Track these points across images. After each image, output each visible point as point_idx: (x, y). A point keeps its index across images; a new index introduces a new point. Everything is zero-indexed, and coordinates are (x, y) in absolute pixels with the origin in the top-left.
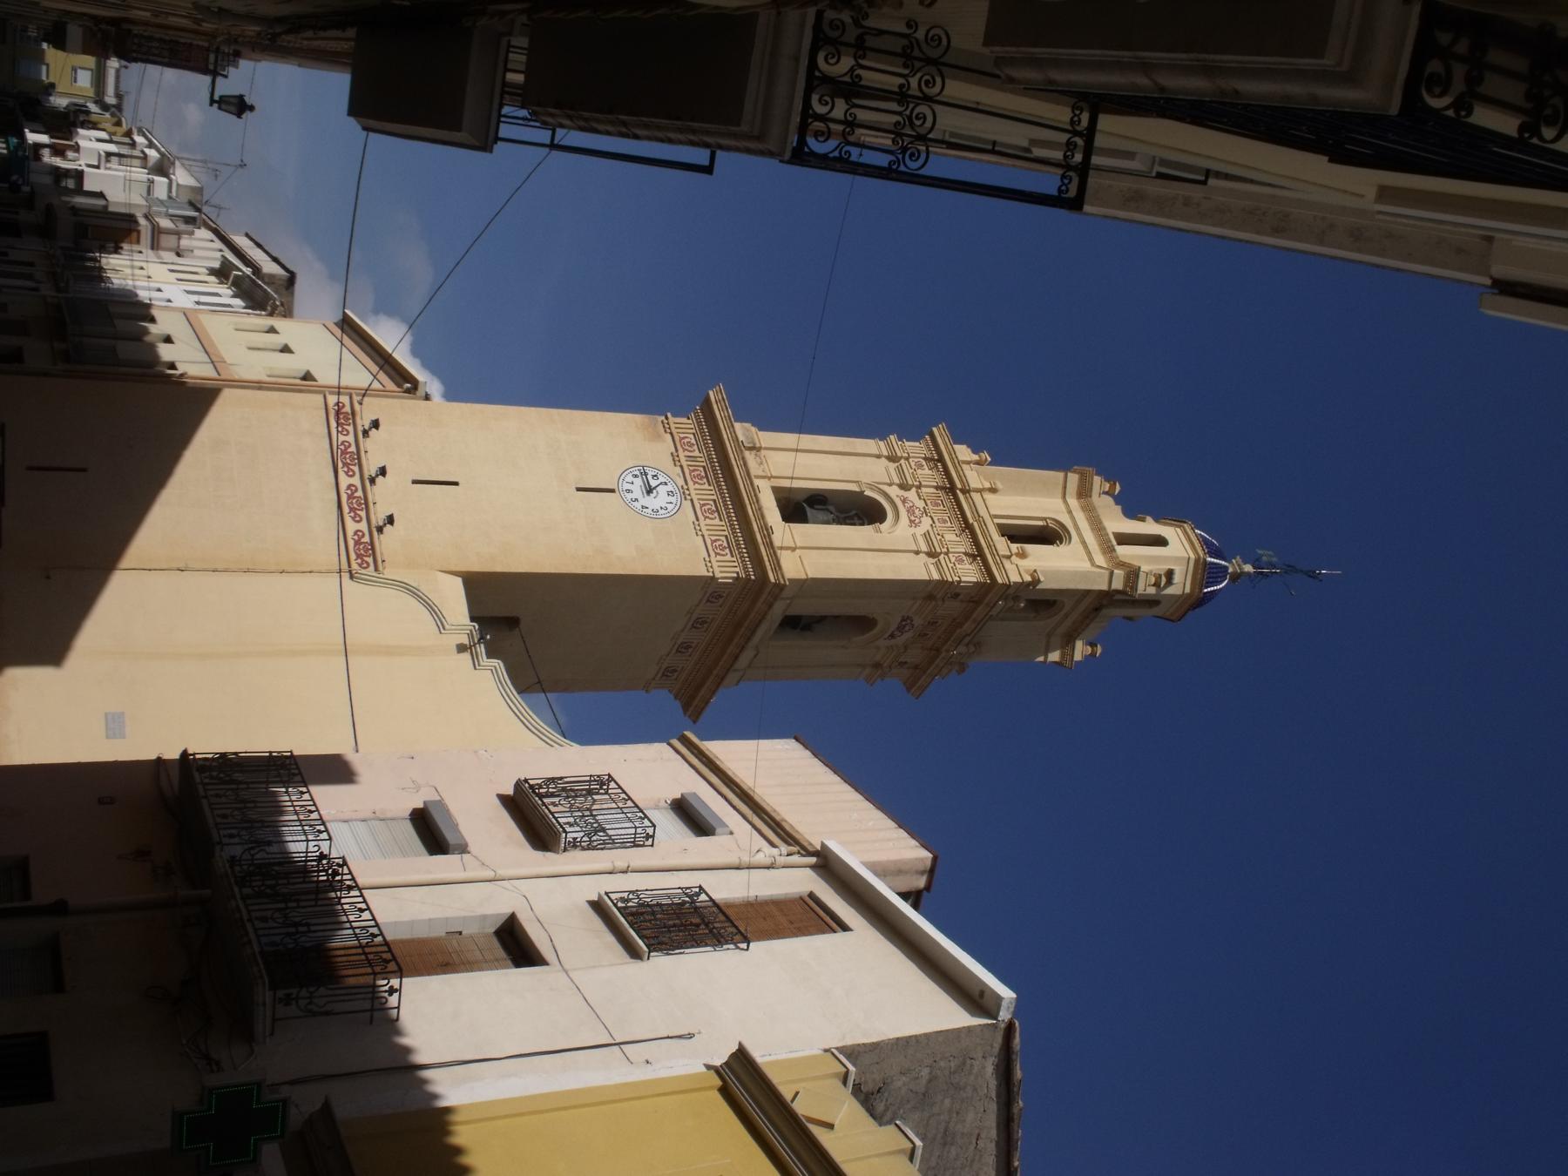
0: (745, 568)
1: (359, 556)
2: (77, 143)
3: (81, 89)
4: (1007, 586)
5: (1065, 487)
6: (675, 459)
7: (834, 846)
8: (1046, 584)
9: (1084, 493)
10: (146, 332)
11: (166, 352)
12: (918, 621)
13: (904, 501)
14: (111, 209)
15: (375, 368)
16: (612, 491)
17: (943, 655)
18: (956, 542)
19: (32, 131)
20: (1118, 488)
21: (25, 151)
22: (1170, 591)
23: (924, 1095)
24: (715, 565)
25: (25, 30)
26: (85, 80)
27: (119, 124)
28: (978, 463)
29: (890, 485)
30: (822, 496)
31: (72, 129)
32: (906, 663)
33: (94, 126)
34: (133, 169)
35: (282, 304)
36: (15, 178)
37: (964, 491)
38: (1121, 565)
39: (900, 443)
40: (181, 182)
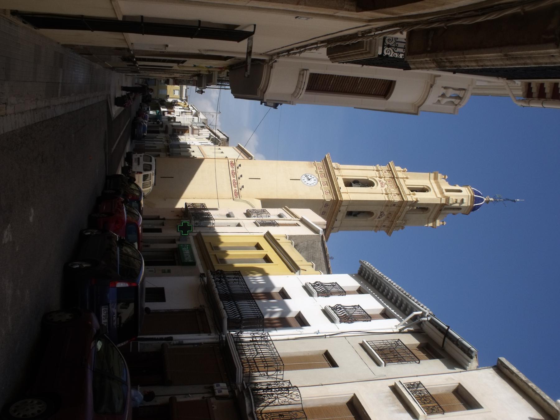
0: (333, 197)
1: (235, 195)
2: (174, 110)
3: (176, 96)
4: (407, 201)
5: (430, 177)
6: (316, 172)
7: (304, 217)
8: (420, 202)
9: (436, 178)
10: (189, 150)
11: (193, 154)
12: (386, 213)
13: (380, 181)
14: (182, 125)
15: (240, 152)
16: (300, 180)
17: (394, 223)
18: (394, 191)
19: (162, 108)
20: (447, 177)
21: (161, 113)
22: (463, 205)
23: (307, 247)
24: (325, 197)
25: (161, 81)
26: (177, 93)
27: (186, 104)
28: (404, 171)
29: (376, 177)
30: (357, 180)
31: (173, 107)
32: (385, 226)
33: (179, 105)
34: (189, 116)
35: (222, 143)
36: (158, 120)
37: (397, 178)
38: (445, 197)
39: (380, 167)
40: (201, 118)
